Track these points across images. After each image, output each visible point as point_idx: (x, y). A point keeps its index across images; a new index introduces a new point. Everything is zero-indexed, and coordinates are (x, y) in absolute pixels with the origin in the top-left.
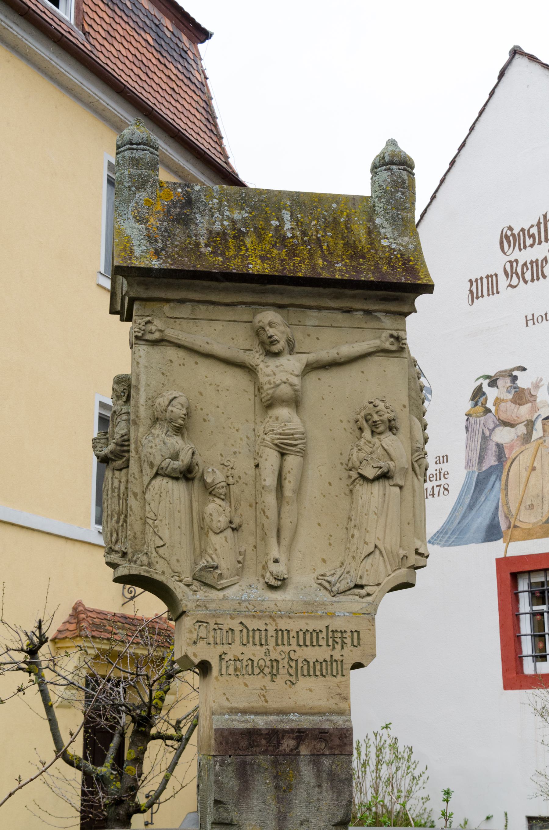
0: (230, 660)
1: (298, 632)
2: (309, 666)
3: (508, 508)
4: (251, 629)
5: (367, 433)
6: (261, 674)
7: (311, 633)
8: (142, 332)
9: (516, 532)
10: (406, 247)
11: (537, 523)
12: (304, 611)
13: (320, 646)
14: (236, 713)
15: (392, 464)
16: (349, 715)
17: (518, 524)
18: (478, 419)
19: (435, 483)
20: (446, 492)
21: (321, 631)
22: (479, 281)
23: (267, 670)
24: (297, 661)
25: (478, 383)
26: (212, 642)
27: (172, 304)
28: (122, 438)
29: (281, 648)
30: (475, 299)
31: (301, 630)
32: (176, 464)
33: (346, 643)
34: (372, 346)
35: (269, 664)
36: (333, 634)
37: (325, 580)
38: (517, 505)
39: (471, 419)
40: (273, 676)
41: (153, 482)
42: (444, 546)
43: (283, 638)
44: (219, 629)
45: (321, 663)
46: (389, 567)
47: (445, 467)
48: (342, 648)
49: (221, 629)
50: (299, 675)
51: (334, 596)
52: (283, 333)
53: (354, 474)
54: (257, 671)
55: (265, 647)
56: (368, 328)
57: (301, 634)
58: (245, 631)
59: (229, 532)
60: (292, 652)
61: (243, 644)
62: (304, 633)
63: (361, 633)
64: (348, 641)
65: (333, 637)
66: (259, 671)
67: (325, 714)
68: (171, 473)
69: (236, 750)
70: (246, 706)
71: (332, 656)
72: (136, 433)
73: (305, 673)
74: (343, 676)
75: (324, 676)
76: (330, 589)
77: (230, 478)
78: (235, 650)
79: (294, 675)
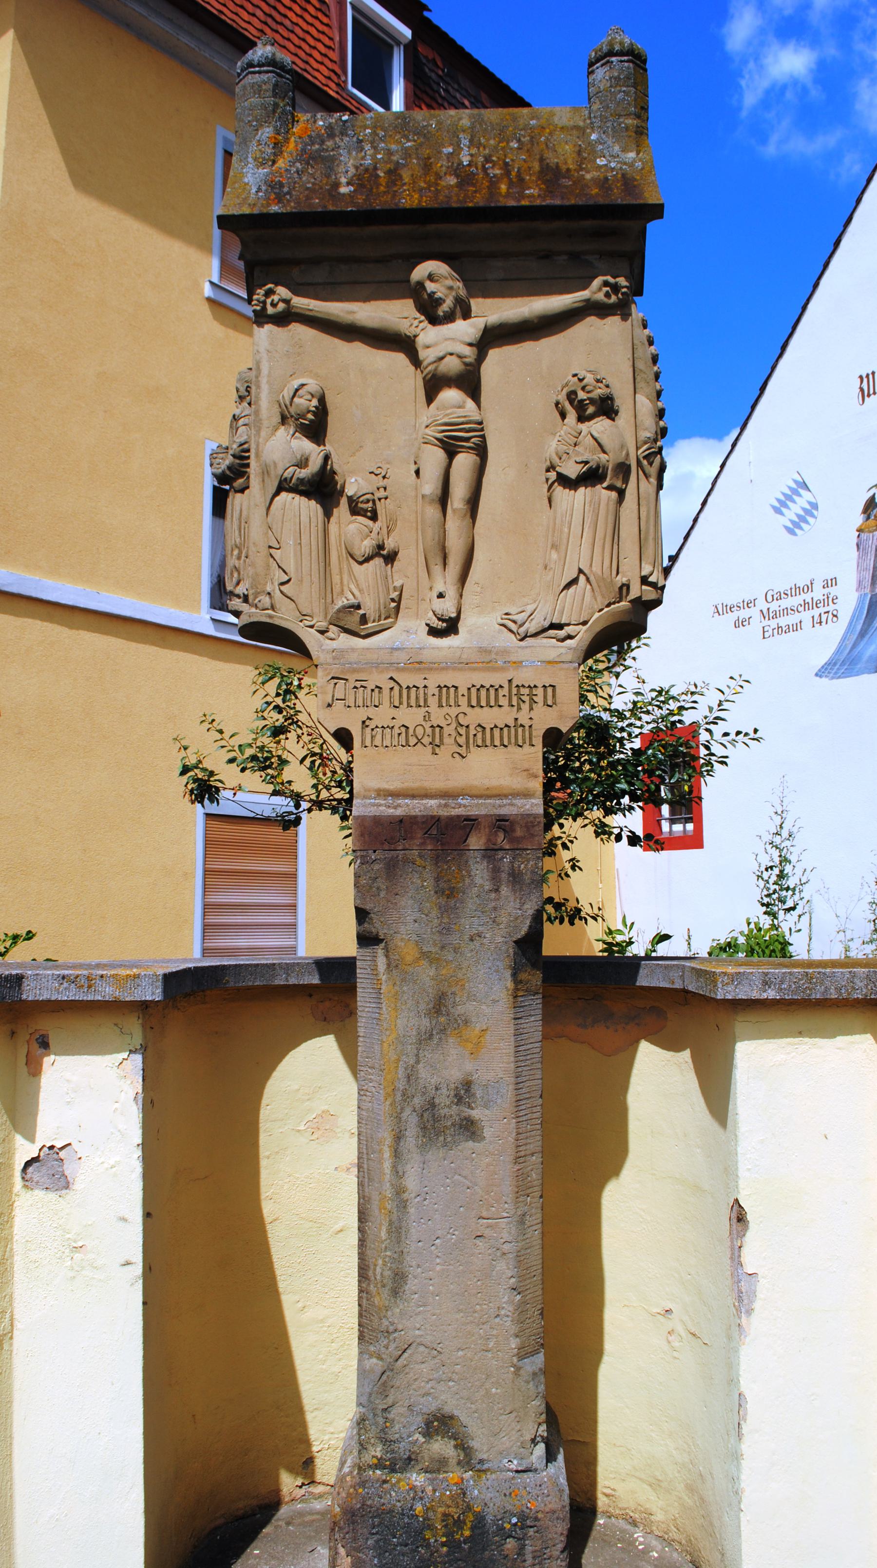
0: (377, 727)
1: (469, 689)
4: (404, 686)
5: (572, 416)
7: (488, 690)
10: (631, 165)
12: (478, 660)
13: (500, 706)
14: (385, 796)
15: (604, 457)
18: (871, 535)
19: (822, 610)
20: (835, 619)
21: (501, 686)
22: (871, 377)
23: (426, 740)
24: (467, 727)
25: (871, 494)
26: (352, 704)
28: (241, 448)
29: (446, 710)
30: (866, 398)
31: (473, 686)
32: (304, 473)
34: (578, 299)
35: (429, 731)
36: (518, 691)
37: (509, 620)
39: (862, 535)
40: (435, 746)
41: (277, 498)
42: (832, 678)
43: (448, 698)
44: (362, 686)
45: (501, 729)
46: (599, 598)
47: (833, 591)
48: (531, 709)
49: (365, 687)
50: (471, 746)
51: (522, 640)
52: (451, 288)
53: (553, 475)
54: (413, 741)
55: (423, 710)
57: (473, 690)
58: (397, 688)
60: (461, 716)
63: (557, 688)
64: (539, 699)
67: (506, 796)
68: (297, 485)
69: (383, 844)
71: (516, 719)
73: (480, 743)
75: (506, 746)
76: (515, 631)
77: (382, 490)
78: (382, 715)
79: (465, 746)
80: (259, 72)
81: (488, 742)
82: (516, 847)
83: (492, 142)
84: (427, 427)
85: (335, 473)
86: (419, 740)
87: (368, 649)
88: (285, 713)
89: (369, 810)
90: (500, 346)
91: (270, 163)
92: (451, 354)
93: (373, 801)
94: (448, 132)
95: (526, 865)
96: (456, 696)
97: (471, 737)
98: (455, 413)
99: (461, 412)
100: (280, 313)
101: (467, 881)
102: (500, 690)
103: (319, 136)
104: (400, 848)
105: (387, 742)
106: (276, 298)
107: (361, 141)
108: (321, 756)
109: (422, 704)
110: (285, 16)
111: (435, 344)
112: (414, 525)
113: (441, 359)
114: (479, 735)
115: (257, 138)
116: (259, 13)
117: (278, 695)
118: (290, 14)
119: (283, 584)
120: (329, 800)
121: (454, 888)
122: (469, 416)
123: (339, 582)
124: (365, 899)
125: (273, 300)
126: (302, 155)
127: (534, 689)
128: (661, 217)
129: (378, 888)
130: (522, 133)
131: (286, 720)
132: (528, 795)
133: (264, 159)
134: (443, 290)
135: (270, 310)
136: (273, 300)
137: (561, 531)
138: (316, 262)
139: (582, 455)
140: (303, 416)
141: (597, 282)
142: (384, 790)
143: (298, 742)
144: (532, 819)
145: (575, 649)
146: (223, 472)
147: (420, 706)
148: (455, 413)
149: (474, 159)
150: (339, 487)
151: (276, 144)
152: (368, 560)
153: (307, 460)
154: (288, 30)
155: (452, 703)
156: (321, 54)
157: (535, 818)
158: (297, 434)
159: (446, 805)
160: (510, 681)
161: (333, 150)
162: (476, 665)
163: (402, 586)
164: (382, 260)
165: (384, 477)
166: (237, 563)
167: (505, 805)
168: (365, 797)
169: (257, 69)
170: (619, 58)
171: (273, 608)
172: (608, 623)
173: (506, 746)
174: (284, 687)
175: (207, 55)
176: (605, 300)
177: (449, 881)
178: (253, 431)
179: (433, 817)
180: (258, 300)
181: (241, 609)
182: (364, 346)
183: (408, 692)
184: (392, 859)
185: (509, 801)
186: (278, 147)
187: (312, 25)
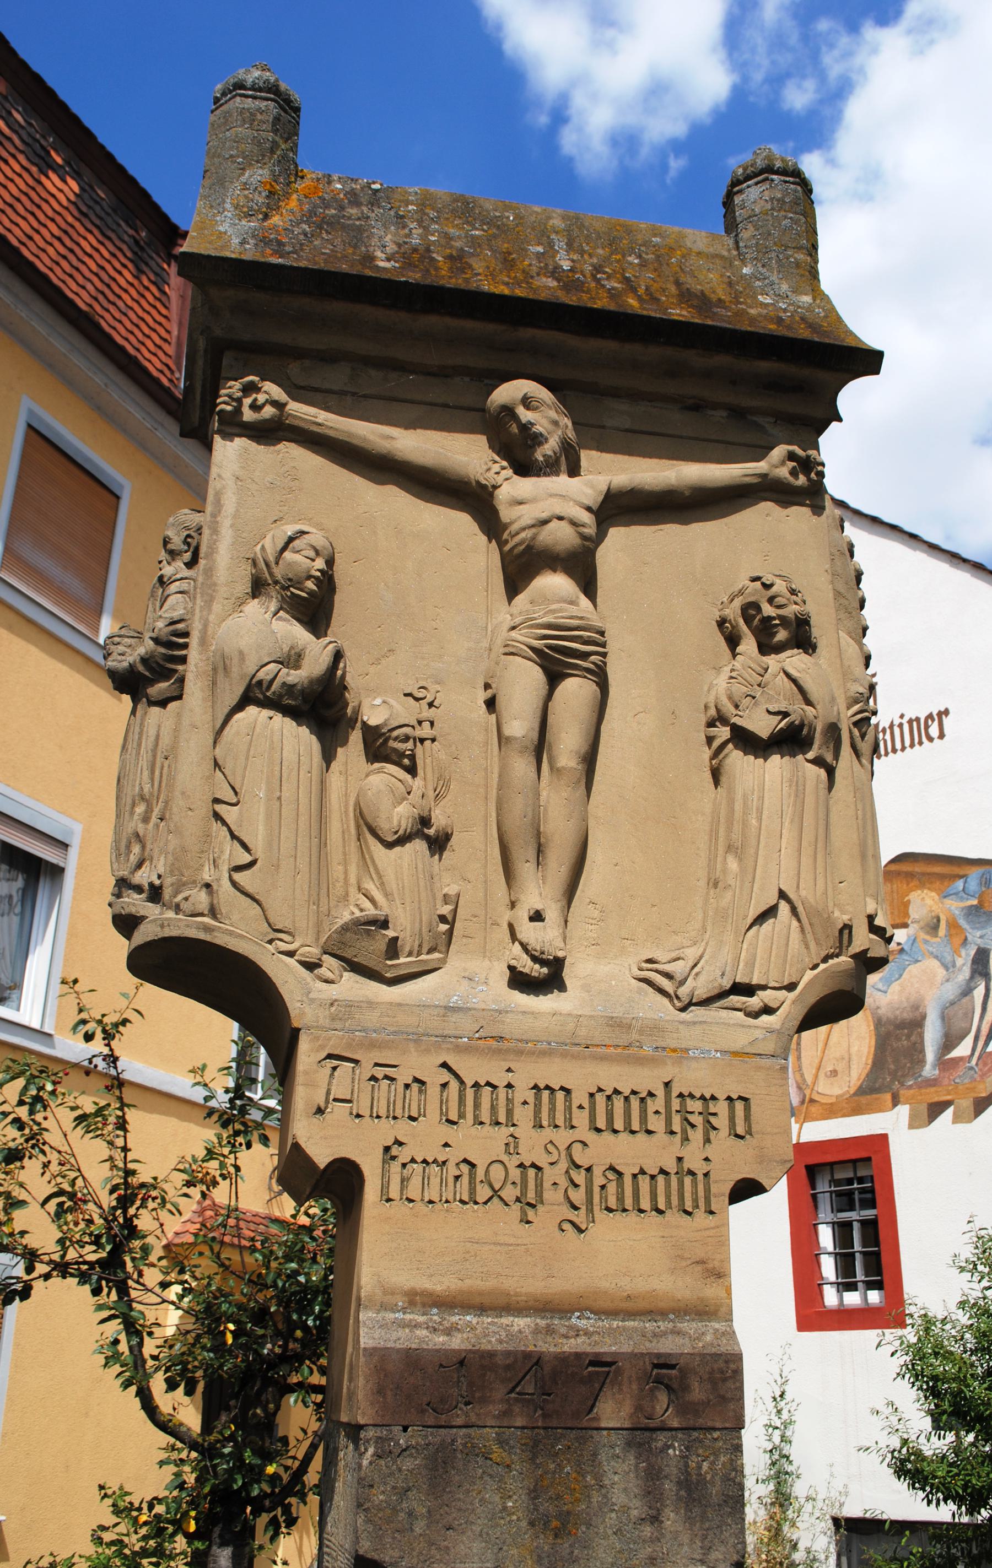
0: (413, 1160)
1: (592, 1095)
2: (620, 1184)
3: (802, 1075)
4: (469, 1083)
5: (749, 645)
6: (495, 1200)
8: (234, 404)
9: (814, 1109)
11: (841, 1096)
12: (607, 1042)
13: (649, 1132)
14: (424, 1305)
16: (729, 1318)
17: (816, 1097)
21: (651, 1094)
23: (510, 1193)
24: (589, 1170)
27: (307, 363)
29: (548, 1133)
31: (600, 1090)
32: (294, 676)
33: (715, 1129)
35: (515, 1174)
36: (683, 1104)
37: (657, 971)
38: (814, 1071)
43: (552, 1110)
45: (653, 1177)
46: (812, 945)
48: (707, 1140)
49: (392, 1079)
50: (596, 1208)
51: (683, 1009)
52: (556, 423)
53: (723, 733)
54: (483, 1193)
55: (505, 1131)
56: (740, 444)
57: (600, 1098)
58: (454, 1085)
59: (419, 845)
60: (577, 1148)
61: (448, 1121)
62: (609, 1098)
64: (721, 1122)
65: (683, 1112)
66: (490, 1193)
68: (281, 696)
69: (423, 1411)
70: (453, 1287)
72: (205, 613)
73: (612, 1203)
74: (712, 1213)
75: (660, 1212)
76: (671, 991)
79: (584, 1208)
80: (255, 98)
81: (629, 1203)
82: (691, 1423)
83: (600, 251)
84: (513, 628)
85: (345, 688)
86: (495, 1191)
87: (400, 1005)
88: (27, 1131)
89: (394, 1335)
90: (627, 524)
91: (261, 216)
92: (560, 518)
93: (399, 1315)
94: (533, 229)
95: (713, 1463)
96: (568, 1109)
97: (596, 1190)
98: (566, 611)
99: (573, 610)
100: (265, 421)
101: (596, 1498)
102: (649, 1100)
103: (334, 199)
104: (459, 1421)
105: (433, 1194)
106: (261, 398)
107: (403, 217)
108: (72, 1196)
109: (502, 1119)
110: (120, 297)
111: (533, 500)
112: (482, 790)
113: (545, 522)
114: (612, 1188)
115: (243, 179)
116: (89, 287)
117: (21, 1103)
118: (124, 296)
119: (239, 868)
120: (78, 1263)
121: (568, 1513)
122: (588, 619)
123: (342, 877)
124: (381, 1538)
125: (256, 400)
126: (311, 216)
127: (711, 1104)
128: (876, 371)
129: (410, 1514)
130: (643, 249)
131: (27, 1141)
132: (706, 1313)
133: (251, 209)
134: (545, 422)
135: (248, 415)
136: (256, 400)
137: (745, 823)
138: (328, 358)
139: (777, 701)
140: (298, 584)
141: (779, 452)
142: (424, 1293)
143: (43, 1174)
144: (721, 1364)
145: (779, 1032)
146: (131, 666)
147: (498, 1123)
148: (566, 611)
149: (578, 266)
150: (349, 711)
151: (272, 193)
152: (402, 840)
153: (299, 656)
154: (120, 311)
155: (560, 1121)
156: (155, 344)
157: (727, 1362)
158: (282, 613)
159: (550, 1331)
160: (667, 1085)
161: (359, 219)
162: (604, 1050)
163: (458, 895)
164: (443, 373)
165: (431, 705)
166: (141, 828)
167: (664, 1334)
168: (384, 1307)
169: (250, 93)
170: (782, 178)
171: (213, 912)
172: (826, 991)
173: (660, 1212)
174: (34, 1092)
175: (23, 315)
176: (791, 479)
177: (559, 1497)
178: (199, 601)
179: (527, 1355)
180: (229, 396)
181: (142, 913)
182: (403, 493)
183: (476, 1093)
184: (442, 1446)
185: (671, 1325)
186: (274, 199)
187: (148, 313)
